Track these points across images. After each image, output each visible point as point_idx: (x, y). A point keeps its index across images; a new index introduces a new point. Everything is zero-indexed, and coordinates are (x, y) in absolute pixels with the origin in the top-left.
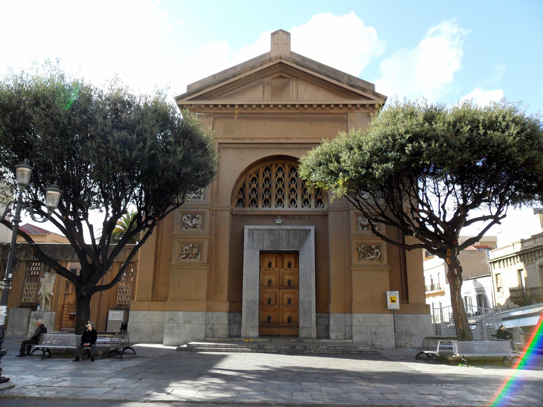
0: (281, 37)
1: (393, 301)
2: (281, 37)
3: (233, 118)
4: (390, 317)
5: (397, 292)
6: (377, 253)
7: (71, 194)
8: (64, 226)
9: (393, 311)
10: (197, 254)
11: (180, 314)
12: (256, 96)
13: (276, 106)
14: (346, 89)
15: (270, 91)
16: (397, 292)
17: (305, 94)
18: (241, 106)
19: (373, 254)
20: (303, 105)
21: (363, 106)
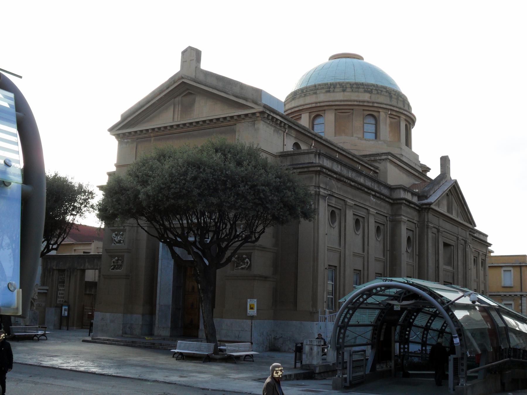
0: (192, 56)
1: (252, 308)
2: (192, 56)
3: (150, 140)
4: (249, 322)
5: (255, 300)
6: (247, 263)
7: (246, 258)
8: (410, 372)
9: (252, 318)
10: (121, 266)
11: (108, 315)
12: (167, 118)
13: (184, 125)
14: (235, 101)
15: (180, 110)
16: (255, 300)
17: (204, 110)
18: (153, 129)
19: (244, 263)
20: (240, 115)
21: (246, 115)
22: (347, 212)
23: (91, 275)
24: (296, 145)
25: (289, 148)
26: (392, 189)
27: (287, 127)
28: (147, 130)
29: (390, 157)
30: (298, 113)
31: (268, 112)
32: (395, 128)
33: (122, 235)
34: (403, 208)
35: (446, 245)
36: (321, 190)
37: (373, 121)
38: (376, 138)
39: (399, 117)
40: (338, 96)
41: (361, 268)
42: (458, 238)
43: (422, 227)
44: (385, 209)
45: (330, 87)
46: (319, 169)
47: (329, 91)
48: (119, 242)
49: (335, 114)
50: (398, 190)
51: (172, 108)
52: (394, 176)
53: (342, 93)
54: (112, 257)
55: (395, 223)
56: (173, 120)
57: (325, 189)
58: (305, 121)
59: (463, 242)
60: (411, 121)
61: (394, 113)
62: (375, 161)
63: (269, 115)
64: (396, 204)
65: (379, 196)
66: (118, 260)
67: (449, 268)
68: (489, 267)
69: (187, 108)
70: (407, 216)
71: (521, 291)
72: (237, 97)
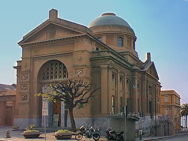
0: (53, 13)
2: (53, 13)
12: (44, 38)
22: (16, 83)
23: (9, 103)
24: (97, 49)
25: (95, 50)
26: (131, 65)
27: (94, 41)
28: (36, 43)
29: (129, 53)
30: (100, 35)
31: (88, 35)
32: (129, 42)
33: (26, 86)
34: (137, 73)
35: (150, 87)
36: (110, 66)
37: (121, 40)
38: (122, 46)
39: (131, 38)
40: (107, 30)
41: (122, 96)
42: (153, 84)
43: (142, 80)
44: (129, 73)
45: (104, 26)
46: (109, 57)
47: (104, 28)
48: (25, 89)
49: (106, 37)
50: (134, 66)
51: (46, 35)
52: (130, 60)
53: (109, 29)
54: (22, 95)
55: (133, 79)
56: (47, 39)
57: (111, 65)
58: (104, 40)
59: (154, 86)
60: (135, 39)
61: (129, 36)
62: (125, 55)
63: (90, 37)
64: (133, 71)
65: (127, 68)
66: (25, 96)
67: (151, 96)
68: (161, 95)
69: (53, 34)
70: (137, 75)
71: (172, 104)
72: (74, 29)
